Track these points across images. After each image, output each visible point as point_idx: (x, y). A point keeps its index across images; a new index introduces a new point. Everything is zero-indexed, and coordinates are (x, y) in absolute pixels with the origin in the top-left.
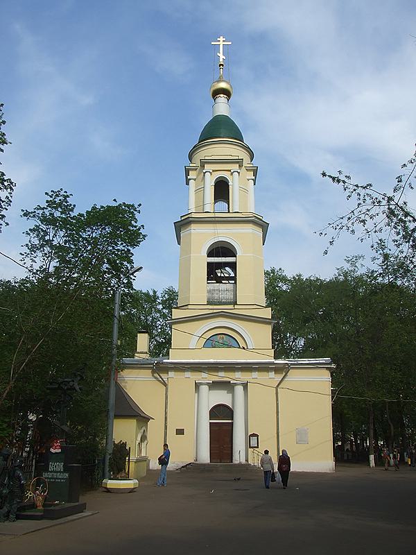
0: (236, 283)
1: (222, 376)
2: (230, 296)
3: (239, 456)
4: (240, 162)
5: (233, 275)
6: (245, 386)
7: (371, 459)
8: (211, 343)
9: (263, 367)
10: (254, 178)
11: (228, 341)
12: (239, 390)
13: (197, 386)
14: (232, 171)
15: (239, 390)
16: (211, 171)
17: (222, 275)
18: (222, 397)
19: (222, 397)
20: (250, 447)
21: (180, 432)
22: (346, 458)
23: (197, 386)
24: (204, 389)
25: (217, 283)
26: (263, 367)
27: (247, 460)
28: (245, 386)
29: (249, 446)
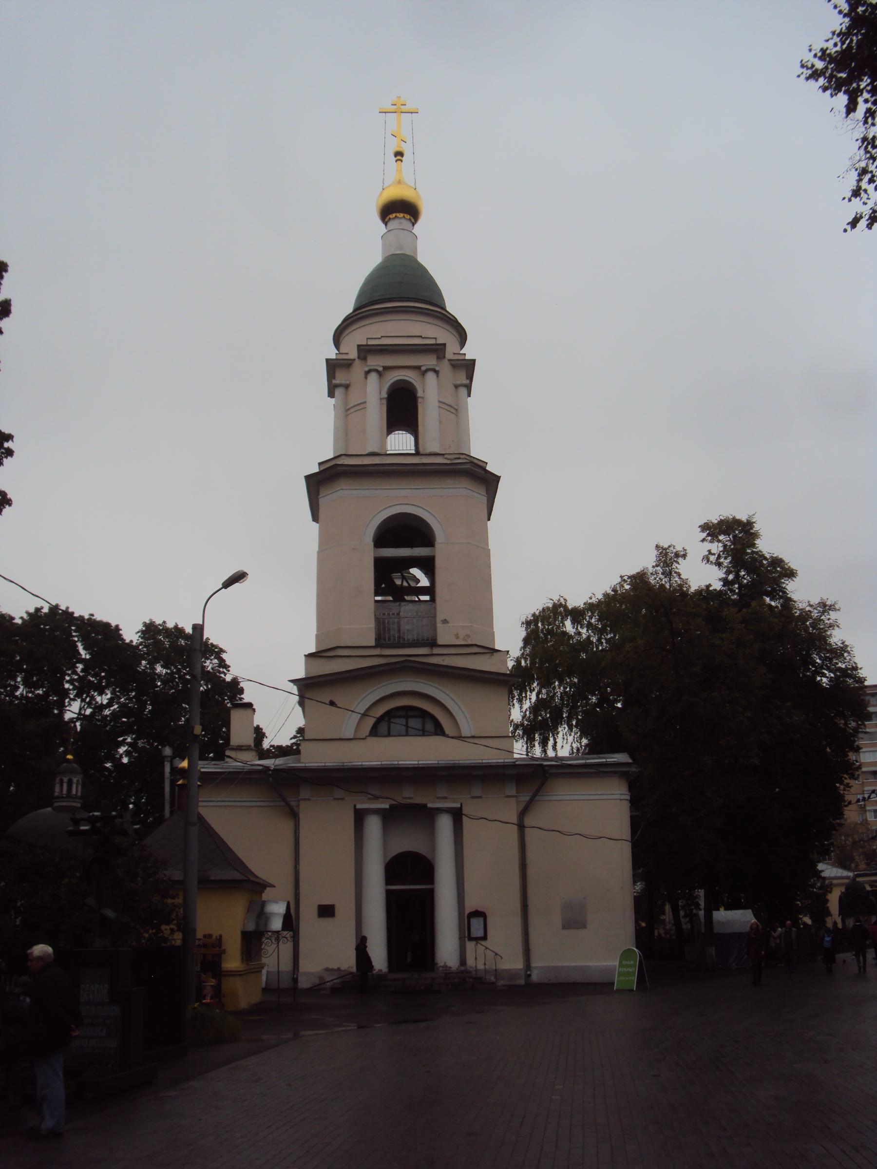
0: (433, 600)
1: (410, 795)
2: (474, 935)
3: (447, 948)
4: (438, 350)
5: (424, 582)
6: (457, 815)
7: (739, 912)
8: (384, 724)
9: (513, 796)
10: (468, 382)
11: (425, 721)
12: (445, 824)
13: (360, 817)
14: (423, 368)
15: (445, 824)
16: (381, 369)
17: (405, 584)
18: (408, 841)
19: (408, 841)
20: (471, 939)
21: (326, 911)
22: (427, 598)
23: (360, 817)
24: (374, 825)
25: (395, 601)
26: (513, 796)
27: (463, 961)
28: (457, 815)
29: (466, 935)
